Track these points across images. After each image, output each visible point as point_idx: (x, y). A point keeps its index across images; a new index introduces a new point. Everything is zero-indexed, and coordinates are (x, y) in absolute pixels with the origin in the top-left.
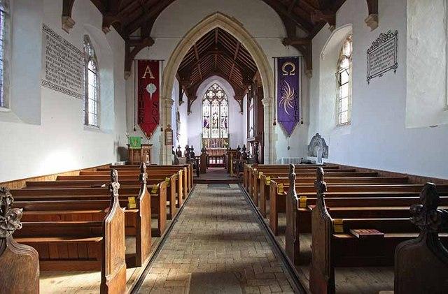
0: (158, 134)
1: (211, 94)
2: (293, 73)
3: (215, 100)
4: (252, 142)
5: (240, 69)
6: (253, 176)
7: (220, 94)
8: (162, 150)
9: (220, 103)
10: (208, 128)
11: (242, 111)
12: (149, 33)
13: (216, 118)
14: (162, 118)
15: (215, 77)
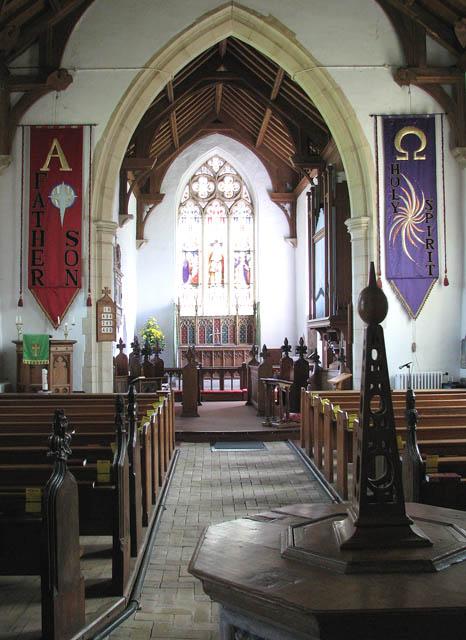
0: (77, 318)
1: (203, 187)
2: (419, 154)
3: (215, 202)
4: (321, 330)
5: (284, 120)
6: (322, 416)
7: (228, 187)
8: (88, 354)
9: (229, 211)
10: (196, 284)
11: (293, 235)
12: (59, 62)
13: (216, 258)
14: (90, 271)
15: (215, 138)
